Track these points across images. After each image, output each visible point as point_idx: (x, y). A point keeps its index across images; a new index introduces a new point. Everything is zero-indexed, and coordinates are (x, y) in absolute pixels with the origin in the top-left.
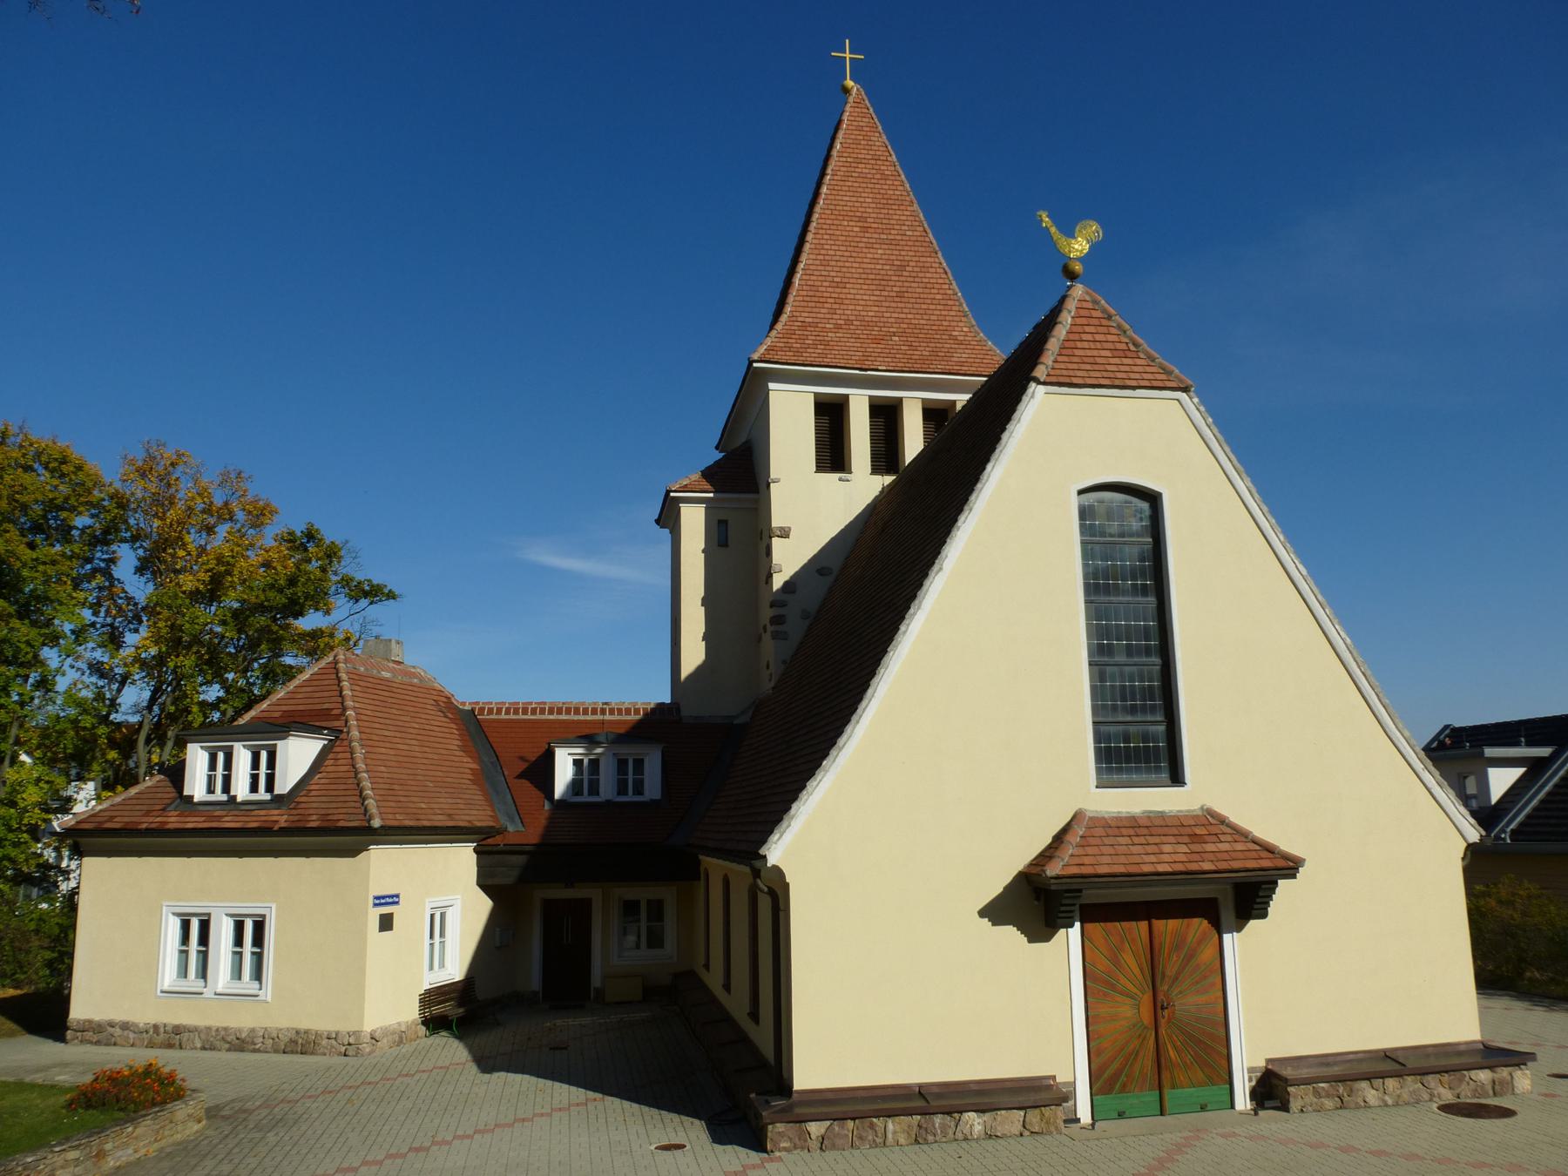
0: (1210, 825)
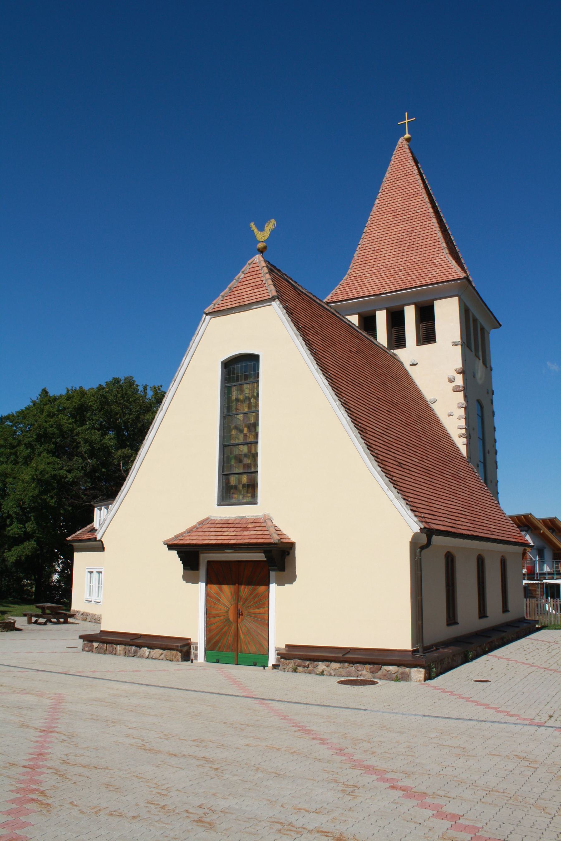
0: (258, 523)
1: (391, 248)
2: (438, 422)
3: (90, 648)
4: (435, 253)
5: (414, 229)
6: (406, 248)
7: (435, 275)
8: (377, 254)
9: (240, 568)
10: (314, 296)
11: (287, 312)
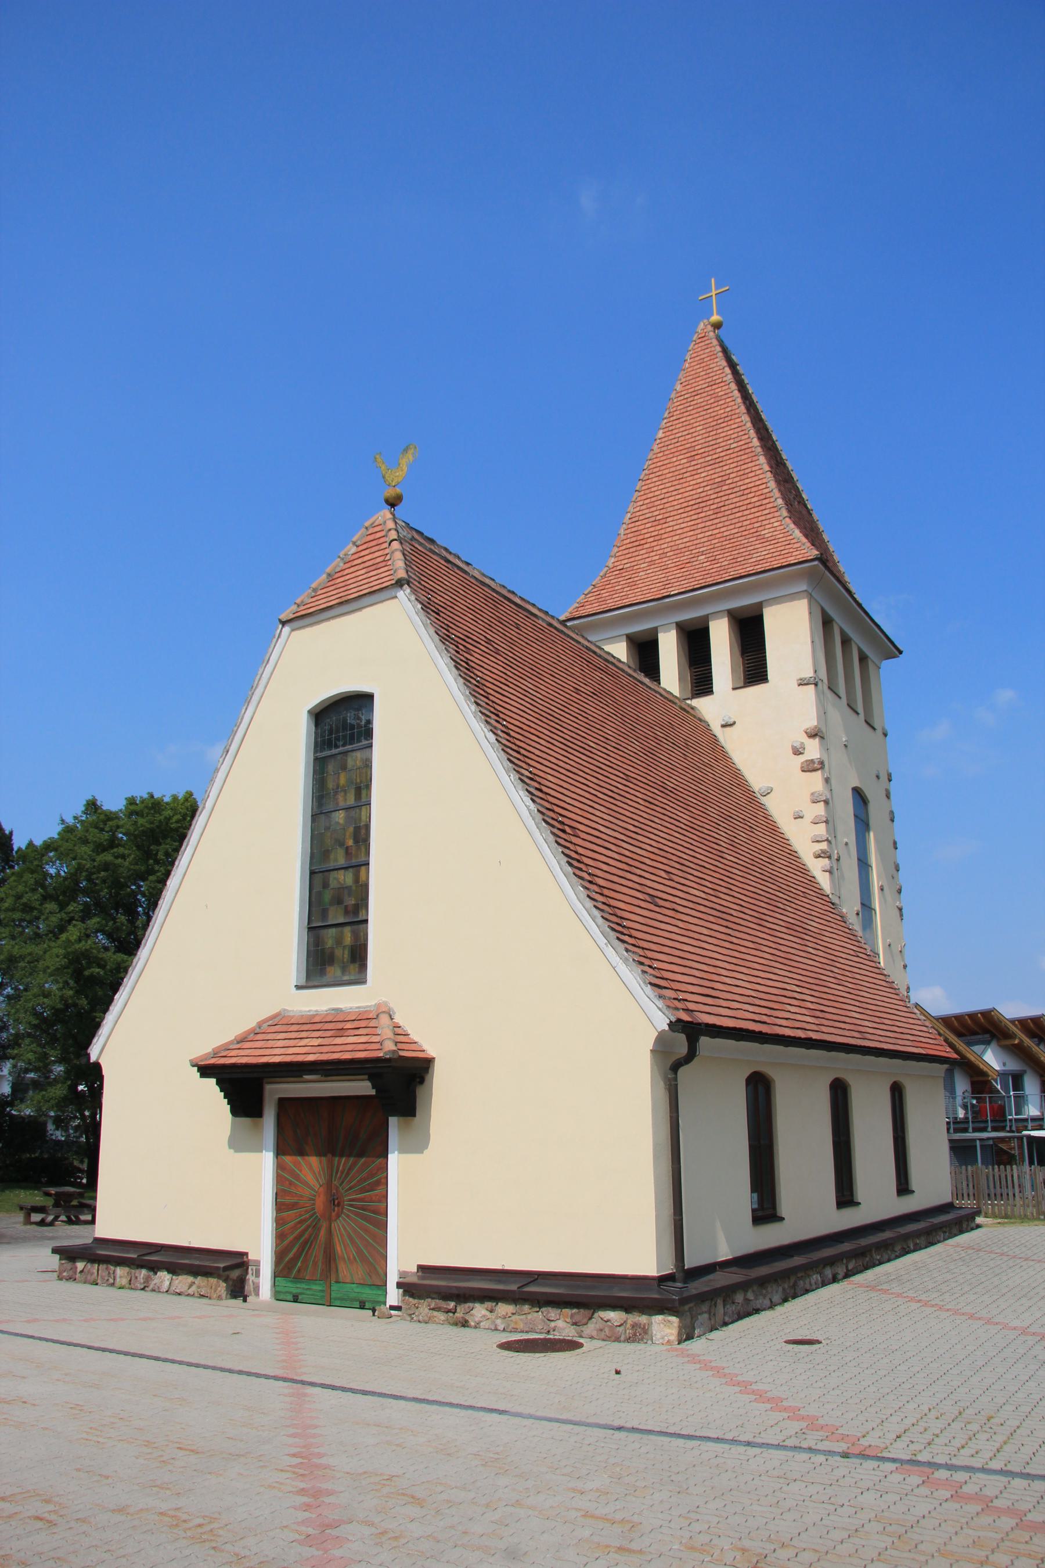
0: (364, 1021)
1: (685, 515)
2: (773, 829)
3: (71, 1273)
4: (763, 518)
5: (724, 478)
6: (711, 512)
7: (763, 556)
8: (659, 527)
9: (336, 1111)
10: (540, 610)
11: (425, 608)
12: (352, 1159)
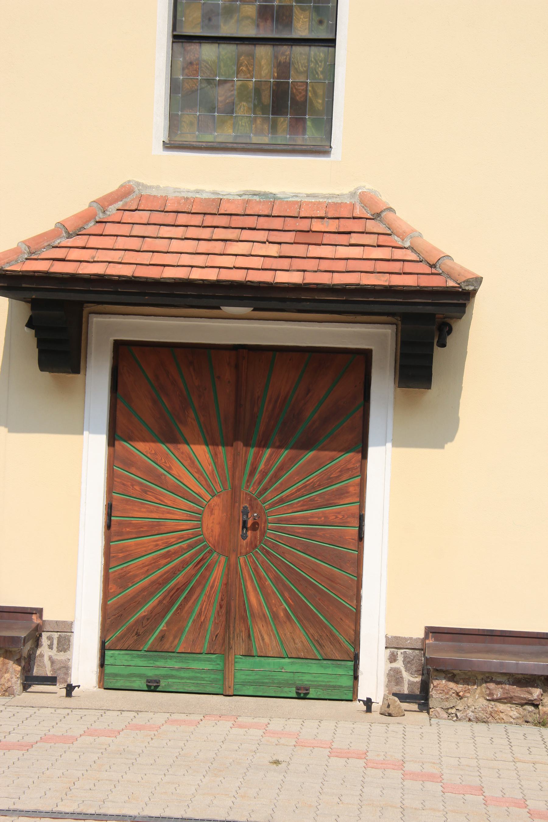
0: (365, 219)
12: (285, 453)
